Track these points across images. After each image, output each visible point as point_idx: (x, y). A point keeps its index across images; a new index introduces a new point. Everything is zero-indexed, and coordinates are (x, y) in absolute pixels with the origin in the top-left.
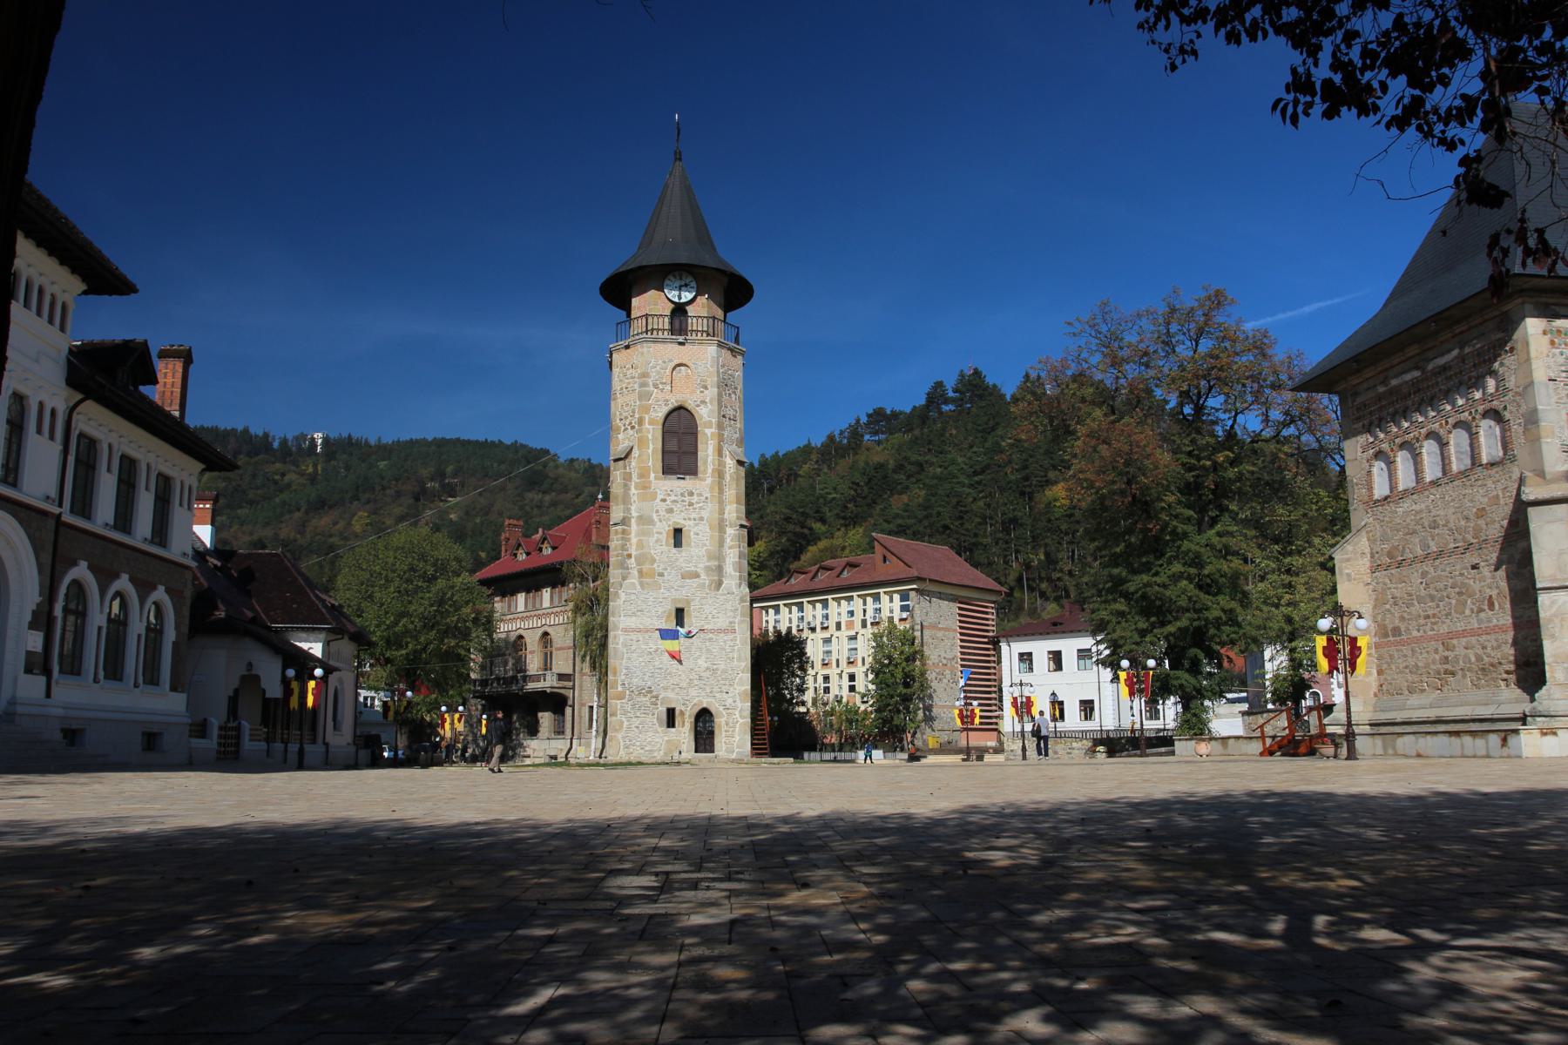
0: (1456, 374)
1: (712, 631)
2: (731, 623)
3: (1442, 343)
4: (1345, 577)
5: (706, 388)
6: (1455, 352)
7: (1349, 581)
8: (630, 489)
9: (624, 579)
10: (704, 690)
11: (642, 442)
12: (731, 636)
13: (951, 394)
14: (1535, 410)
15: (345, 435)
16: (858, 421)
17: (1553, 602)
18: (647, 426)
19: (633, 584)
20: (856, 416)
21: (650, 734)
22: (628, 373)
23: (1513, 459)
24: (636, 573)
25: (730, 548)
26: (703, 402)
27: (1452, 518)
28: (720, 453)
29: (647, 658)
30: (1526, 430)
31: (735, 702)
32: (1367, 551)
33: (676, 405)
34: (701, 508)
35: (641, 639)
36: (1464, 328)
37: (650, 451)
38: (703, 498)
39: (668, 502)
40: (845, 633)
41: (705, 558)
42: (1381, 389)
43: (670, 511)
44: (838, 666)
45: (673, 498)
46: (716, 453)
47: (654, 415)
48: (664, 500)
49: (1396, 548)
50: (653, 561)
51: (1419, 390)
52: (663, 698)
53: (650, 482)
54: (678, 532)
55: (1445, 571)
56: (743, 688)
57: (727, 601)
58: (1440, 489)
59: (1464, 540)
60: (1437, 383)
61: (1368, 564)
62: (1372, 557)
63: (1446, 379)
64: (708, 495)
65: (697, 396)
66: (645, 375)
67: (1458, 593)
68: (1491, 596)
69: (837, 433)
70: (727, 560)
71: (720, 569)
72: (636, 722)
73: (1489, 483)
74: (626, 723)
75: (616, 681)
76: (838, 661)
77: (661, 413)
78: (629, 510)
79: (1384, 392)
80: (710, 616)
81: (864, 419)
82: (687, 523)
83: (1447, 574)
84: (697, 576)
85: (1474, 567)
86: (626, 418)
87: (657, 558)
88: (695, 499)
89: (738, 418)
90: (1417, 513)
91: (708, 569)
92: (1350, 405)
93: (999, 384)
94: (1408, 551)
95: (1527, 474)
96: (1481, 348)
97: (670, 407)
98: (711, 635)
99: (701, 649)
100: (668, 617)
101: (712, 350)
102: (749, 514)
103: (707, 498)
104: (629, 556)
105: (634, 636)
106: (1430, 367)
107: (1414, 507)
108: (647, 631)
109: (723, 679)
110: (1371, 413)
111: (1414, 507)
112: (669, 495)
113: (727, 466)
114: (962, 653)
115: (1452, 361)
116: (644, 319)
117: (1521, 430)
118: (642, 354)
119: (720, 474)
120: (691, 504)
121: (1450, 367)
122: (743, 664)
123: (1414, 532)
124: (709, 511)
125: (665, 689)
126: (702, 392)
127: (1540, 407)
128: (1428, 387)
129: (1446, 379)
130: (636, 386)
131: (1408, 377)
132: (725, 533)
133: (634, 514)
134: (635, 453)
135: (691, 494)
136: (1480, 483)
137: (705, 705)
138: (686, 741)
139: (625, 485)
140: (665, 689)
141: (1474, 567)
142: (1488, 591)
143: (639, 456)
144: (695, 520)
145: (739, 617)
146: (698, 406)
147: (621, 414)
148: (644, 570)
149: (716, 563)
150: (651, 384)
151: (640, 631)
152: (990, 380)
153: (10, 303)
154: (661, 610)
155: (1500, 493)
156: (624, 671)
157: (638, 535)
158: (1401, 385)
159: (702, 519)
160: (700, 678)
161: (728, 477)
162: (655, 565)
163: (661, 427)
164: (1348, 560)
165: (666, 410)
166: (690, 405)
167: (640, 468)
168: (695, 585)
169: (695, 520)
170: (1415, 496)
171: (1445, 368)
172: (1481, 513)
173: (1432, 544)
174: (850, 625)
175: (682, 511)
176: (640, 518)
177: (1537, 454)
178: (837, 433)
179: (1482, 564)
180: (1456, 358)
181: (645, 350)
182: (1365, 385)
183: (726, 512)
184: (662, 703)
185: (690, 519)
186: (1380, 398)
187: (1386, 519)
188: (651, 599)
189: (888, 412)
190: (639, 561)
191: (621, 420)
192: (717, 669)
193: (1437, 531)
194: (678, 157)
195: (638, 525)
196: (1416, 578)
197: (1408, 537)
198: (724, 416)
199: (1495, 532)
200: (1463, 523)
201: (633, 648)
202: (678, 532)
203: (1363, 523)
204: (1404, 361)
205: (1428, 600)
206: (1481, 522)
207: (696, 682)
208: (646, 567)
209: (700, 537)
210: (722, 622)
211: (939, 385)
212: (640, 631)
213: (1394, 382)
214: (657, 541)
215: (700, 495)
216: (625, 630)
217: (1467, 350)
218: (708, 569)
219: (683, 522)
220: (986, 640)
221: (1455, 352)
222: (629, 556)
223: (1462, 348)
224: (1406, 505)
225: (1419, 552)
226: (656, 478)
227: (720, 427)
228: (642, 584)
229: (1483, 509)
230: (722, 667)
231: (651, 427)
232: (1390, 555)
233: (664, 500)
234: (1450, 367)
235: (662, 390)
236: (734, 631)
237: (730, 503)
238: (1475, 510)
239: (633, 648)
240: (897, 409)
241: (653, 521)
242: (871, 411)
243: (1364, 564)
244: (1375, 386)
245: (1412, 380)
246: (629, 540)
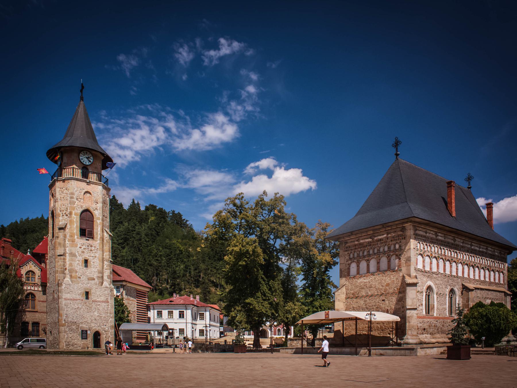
0: (384, 242)
1: (99, 301)
2: (107, 299)
3: (381, 232)
4: (338, 300)
5: (97, 203)
6: (385, 236)
7: (339, 301)
8: (66, 242)
10: (97, 324)
11: (71, 222)
14: (410, 257)
17: (410, 312)
22: (64, 191)
23: (401, 270)
24: (69, 276)
25: (106, 269)
26: (96, 209)
27: (377, 285)
29: (74, 311)
30: (406, 263)
31: (108, 329)
32: (345, 292)
33: (85, 208)
36: (389, 229)
37: (75, 226)
39: (82, 249)
41: (97, 273)
42: (356, 243)
43: (83, 252)
45: (84, 247)
46: (101, 231)
47: (76, 211)
48: (81, 248)
49: (356, 292)
50: (76, 272)
51: (370, 245)
52: (81, 327)
53: (75, 239)
54: (86, 261)
55: (373, 301)
57: (105, 290)
58: (374, 276)
59: (381, 292)
60: (377, 244)
61: (345, 296)
62: (347, 294)
63: (381, 243)
64: (98, 247)
66: (72, 194)
67: (377, 308)
68: (388, 309)
70: (105, 274)
71: (102, 277)
73: (392, 276)
74: (66, 336)
75: (62, 319)
77: (79, 211)
78: (65, 250)
79: (357, 244)
80: (99, 296)
82: (90, 258)
83: (373, 302)
84: (94, 279)
85: (383, 300)
86: (63, 211)
87: (78, 271)
88: (93, 248)
89: (108, 217)
90: (365, 282)
91: (98, 277)
92: (344, 246)
94: (360, 294)
95: (405, 275)
96: (394, 235)
97: (83, 209)
99: (96, 308)
100: (83, 295)
102: (113, 256)
103: (98, 249)
105: (69, 302)
106: (376, 238)
107: (364, 281)
108: (74, 300)
109: (104, 320)
110: (351, 250)
111: (364, 281)
112: (83, 246)
114: (137, 310)
115: (384, 238)
116: (72, 169)
117: (404, 262)
118: (72, 184)
119: (102, 239)
120: (91, 250)
121: (383, 240)
123: (363, 288)
124: (99, 254)
125: (82, 323)
126: (96, 205)
127: (411, 256)
128: (374, 245)
129: (381, 243)
130: (69, 198)
131: (367, 240)
132: (104, 263)
133: (67, 251)
134: (68, 226)
135: (92, 246)
136: (388, 276)
138: (90, 343)
139: (64, 239)
141: (383, 300)
142: (387, 307)
143: (70, 228)
144: (93, 257)
146: (94, 210)
147: (60, 209)
148: (73, 275)
149: (101, 275)
150: (75, 198)
151: (71, 300)
153: (299, 168)
154: (80, 292)
155: (395, 280)
157: (69, 260)
158: (364, 243)
159: (95, 257)
160: (95, 319)
161: (105, 241)
162: (77, 274)
163: (79, 217)
164: (339, 295)
165: (81, 210)
166: (91, 210)
167: (71, 233)
168: (93, 283)
169: (93, 257)
170: (364, 277)
171: (381, 240)
172: (388, 285)
173: (369, 292)
175: (88, 253)
177: (409, 270)
179: (386, 300)
180: (385, 237)
181: (73, 183)
182: (350, 240)
184: (80, 329)
185: (91, 256)
186: (355, 245)
187: (354, 283)
188: (76, 287)
190: (70, 271)
191: (61, 211)
192: (102, 316)
193: (371, 289)
194: (82, 99)
195: (70, 256)
196: (362, 302)
197: (361, 290)
198: (104, 216)
199: (392, 291)
200: (381, 287)
201: (69, 306)
202: (86, 261)
203: (345, 284)
204: (366, 235)
205: (366, 309)
206: (387, 288)
209: (95, 264)
210: (103, 298)
212: (71, 300)
213: (361, 241)
214: (78, 264)
215: (95, 247)
216: (65, 299)
217: (389, 235)
218: (98, 277)
219: (88, 257)
220: (145, 305)
221: (385, 236)
223: (388, 234)
224: (361, 280)
225: (364, 294)
226: (77, 238)
227: (103, 220)
229: (389, 284)
230: (104, 316)
232: (353, 294)
233: (81, 248)
234: (383, 240)
235: (80, 201)
236: (108, 302)
237: (106, 252)
238: (385, 284)
239: (69, 306)
241: (76, 255)
243: (343, 296)
244: (355, 241)
245: (368, 242)
246: (66, 262)
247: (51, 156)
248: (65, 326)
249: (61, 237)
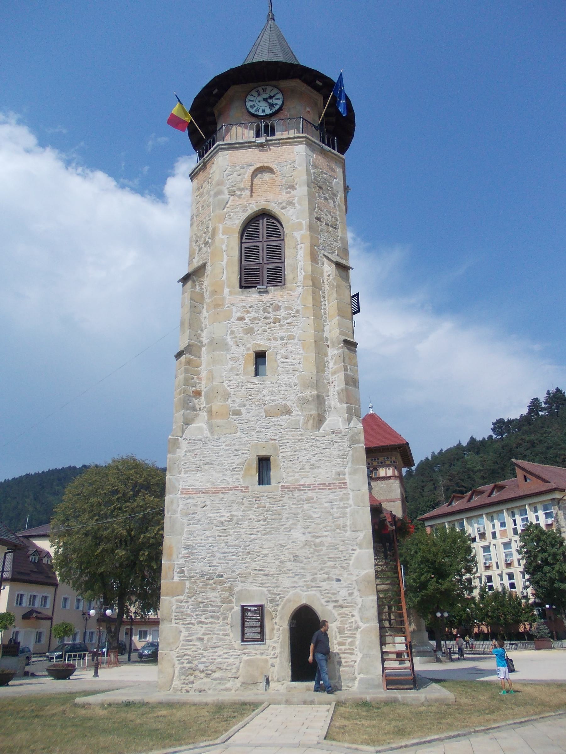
9: (187, 422)
12: (341, 493)
18: (221, 236)
19: (200, 428)
21: (220, 651)
28: (314, 258)
31: (351, 594)
35: (208, 503)
39: (247, 321)
40: (500, 540)
41: (298, 388)
43: (250, 331)
44: (498, 567)
45: (253, 315)
48: (241, 319)
50: (227, 396)
52: (240, 592)
53: (224, 299)
56: (363, 573)
57: (332, 443)
64: (300, 308)
65: (283, 197)
71: (320, 400)
72: (200, 631)
76: (497, 563)
80: (307, 467)
84: (287, 411)
88: (283, 313)
91: (303, 401)
98: (310, 494)
101: (301, 149)
103: (298, 311)
104: (198, 394)
105: (198, 500)
108: (217, 491)
112: (248, 312)
113: (325, 274)
122: (361, 535)
125: (243, 577)
126: (287, 193)
132: (326, 355)
133: (205, 341)
135: (277, 308)
137: (304, 602)
140: (243, 577)
144: (282, 339)
145: (350, 464)
149: (314, 393)
154: (238, 460)
156: (184, 552)
159: (292, 338)
169: (282, 339)
174: (503, 534)
176: (211, 342)
183: (326, 328)
185: (275, 339)
188: (224, 446)
189: (506, 421)
192: (321, 544)
201: (197, 517)
202: (264, 478)
207: (289, 565)
208: (216, 405)
211: (536, 400)
214: (231, 370)
215: (288, 308)
216: (186, 492)
222: (198, 394)
226: (231, 293)
228: (211, 429)
231: (223, 237)
233: (241, 319)
235: (239, 196)
241: (227, 344)
242: (495, 421)
246: (198, 373)
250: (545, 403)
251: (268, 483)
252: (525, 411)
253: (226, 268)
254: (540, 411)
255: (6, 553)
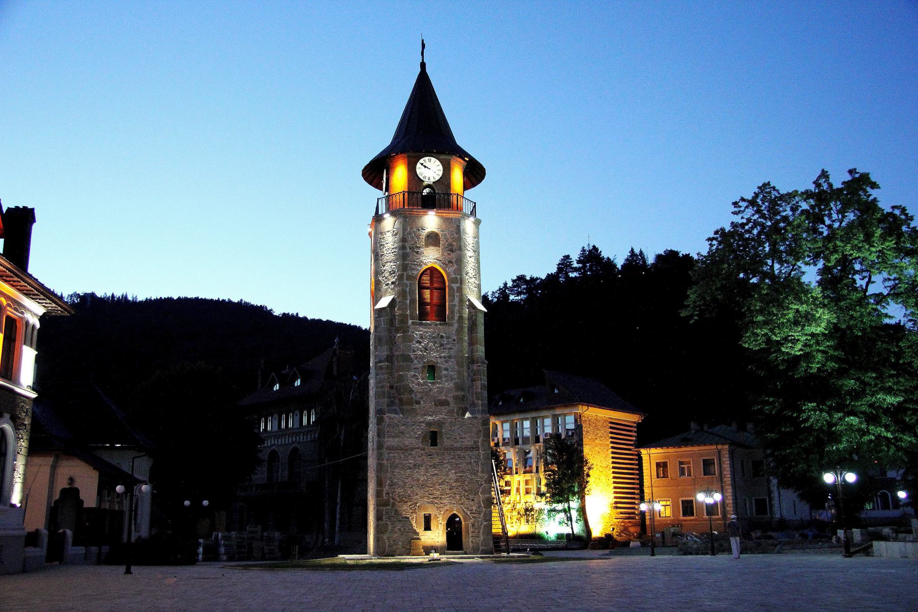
1: (460, 449)
13: (575, 265)
15: (109, 294)
16: (506, 284)
18: (405, 281)
20: (504, 282)
34: (450, 349)
38: (451, 340)
50: (411, 391)
64: (455, 338)
69: (490, 294)
81: (510, 284)
91: (456, 398)
93: (612, 258)
103: (454, 340)
120: (442, 345)
126: (449, 254)
152: (605, 254)
178: (490, 294)
189: (528, 278)
202: (434, 443)
210: (468, 442)
211: (567, 257)
216: (388, 448)
218: (456, 398)
240: (535, 276)
242: (515, 278)
247: (370, 175)
248: (389, 505)
249: (383, 326)
250: (578, 262)
251: (430, 530)
252: (553, 270)
253: (410, 306)
254: (571, 272)
255: (133, 459)
